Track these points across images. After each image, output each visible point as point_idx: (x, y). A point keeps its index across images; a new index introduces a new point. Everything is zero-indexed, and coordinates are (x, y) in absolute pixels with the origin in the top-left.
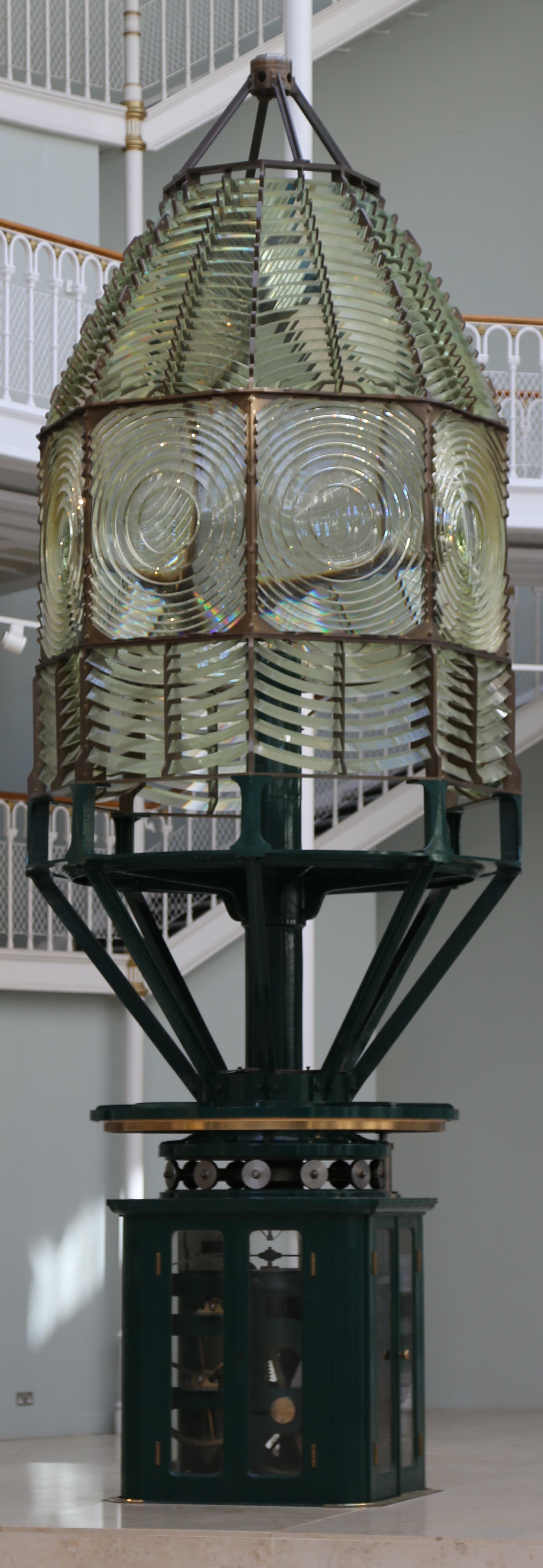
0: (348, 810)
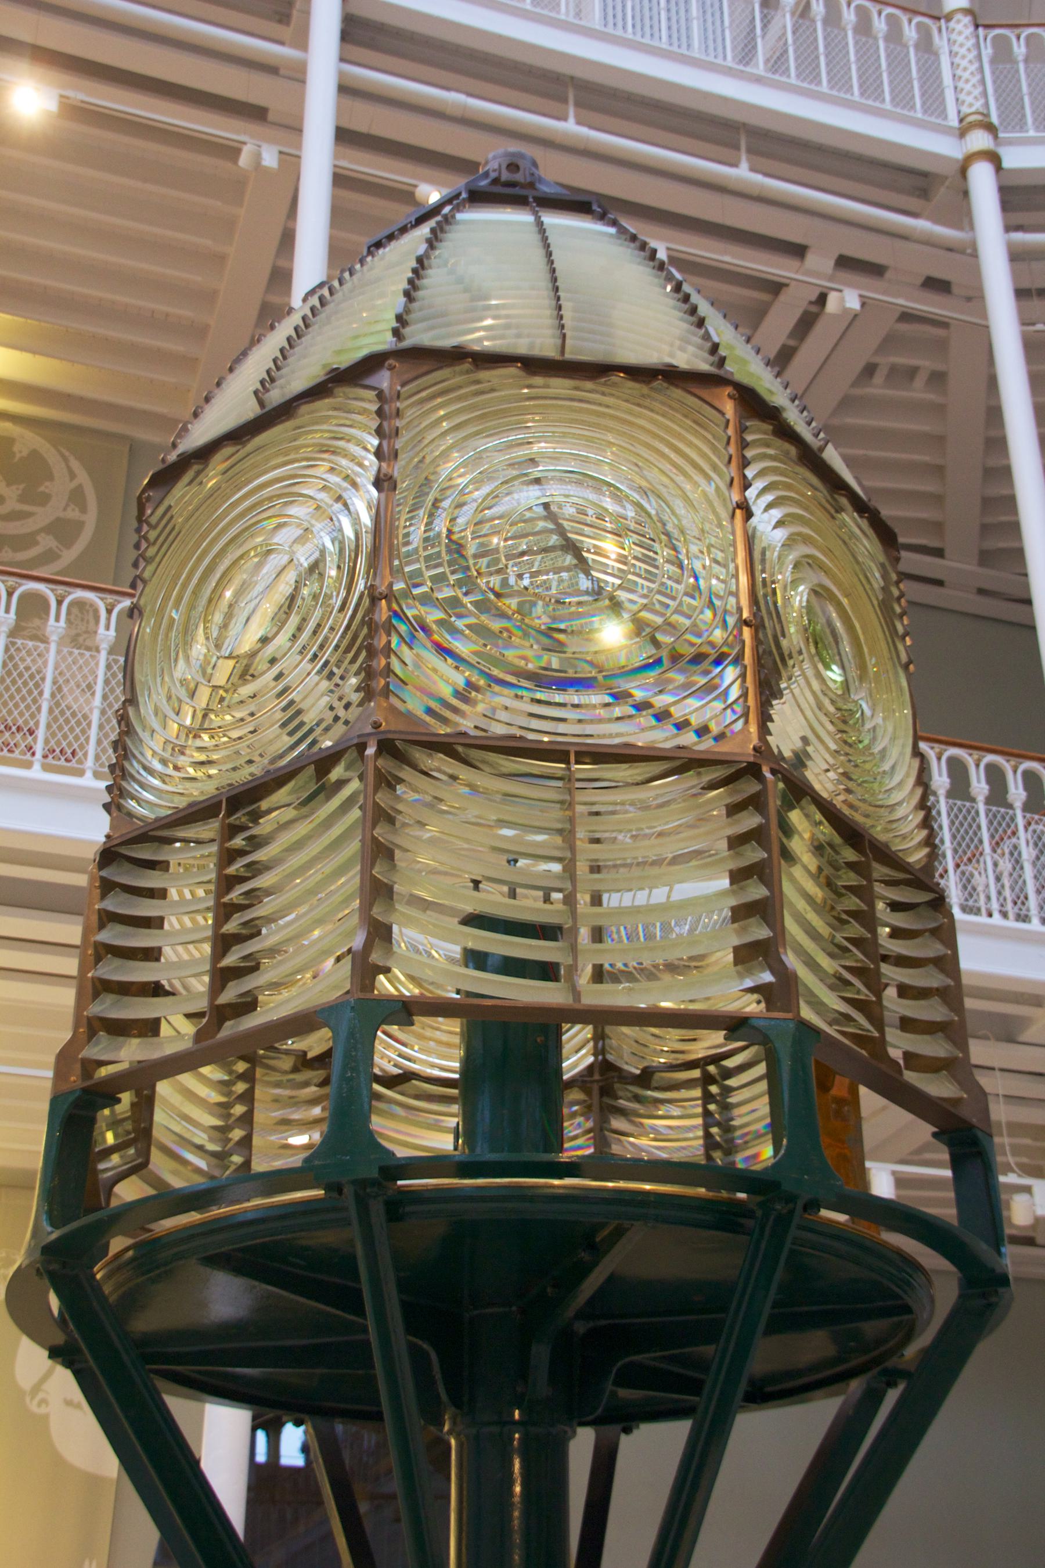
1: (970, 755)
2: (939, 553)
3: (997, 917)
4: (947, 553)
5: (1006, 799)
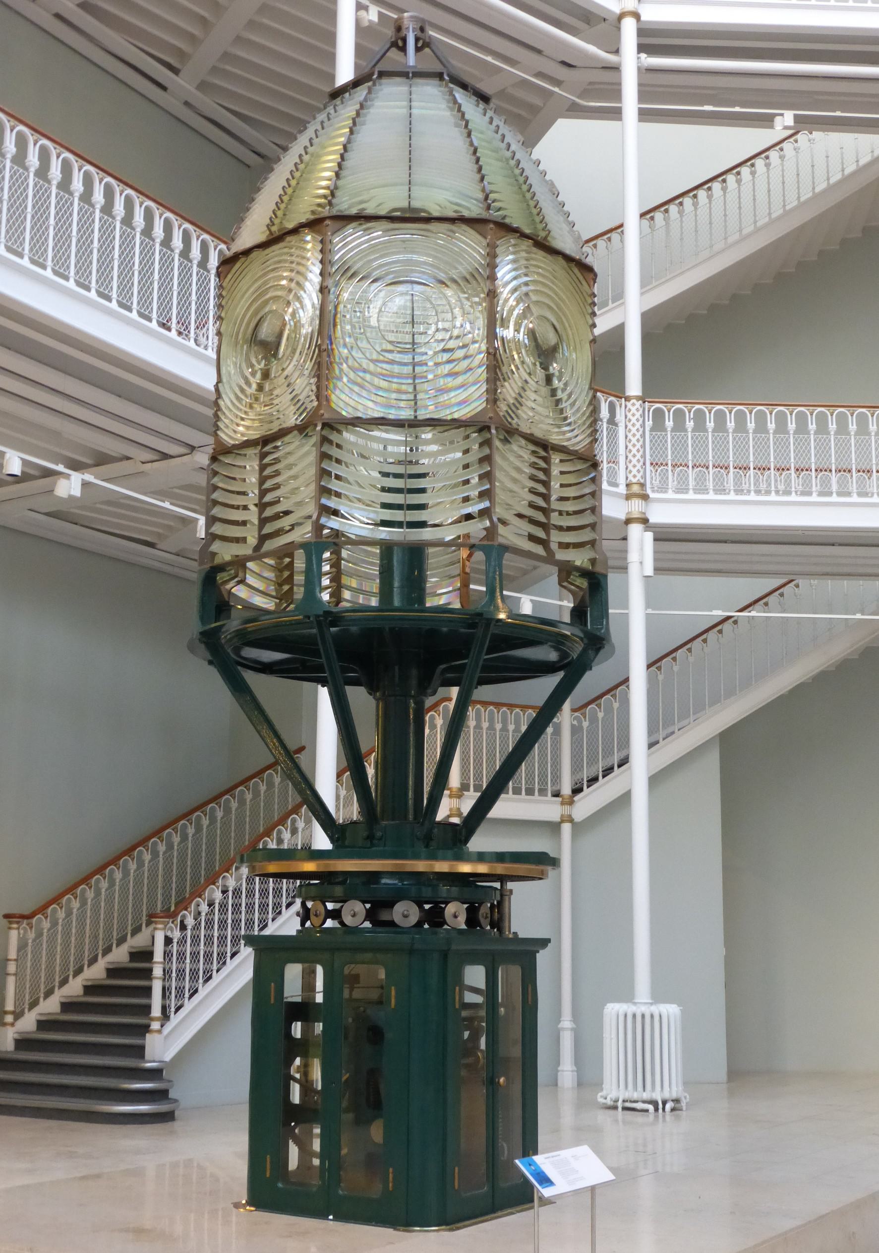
0: (593, 780)
1: (9, 121)
2: (175, 71)
3: (192, 344)
4: (181, 74)
5: (91, 200)
